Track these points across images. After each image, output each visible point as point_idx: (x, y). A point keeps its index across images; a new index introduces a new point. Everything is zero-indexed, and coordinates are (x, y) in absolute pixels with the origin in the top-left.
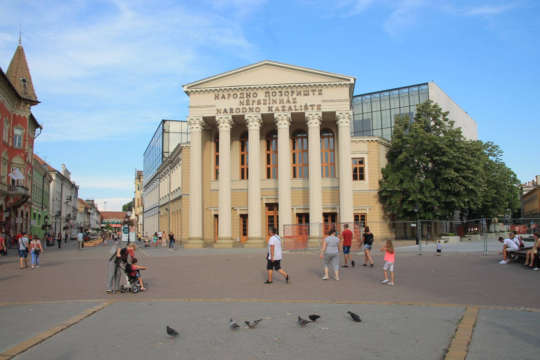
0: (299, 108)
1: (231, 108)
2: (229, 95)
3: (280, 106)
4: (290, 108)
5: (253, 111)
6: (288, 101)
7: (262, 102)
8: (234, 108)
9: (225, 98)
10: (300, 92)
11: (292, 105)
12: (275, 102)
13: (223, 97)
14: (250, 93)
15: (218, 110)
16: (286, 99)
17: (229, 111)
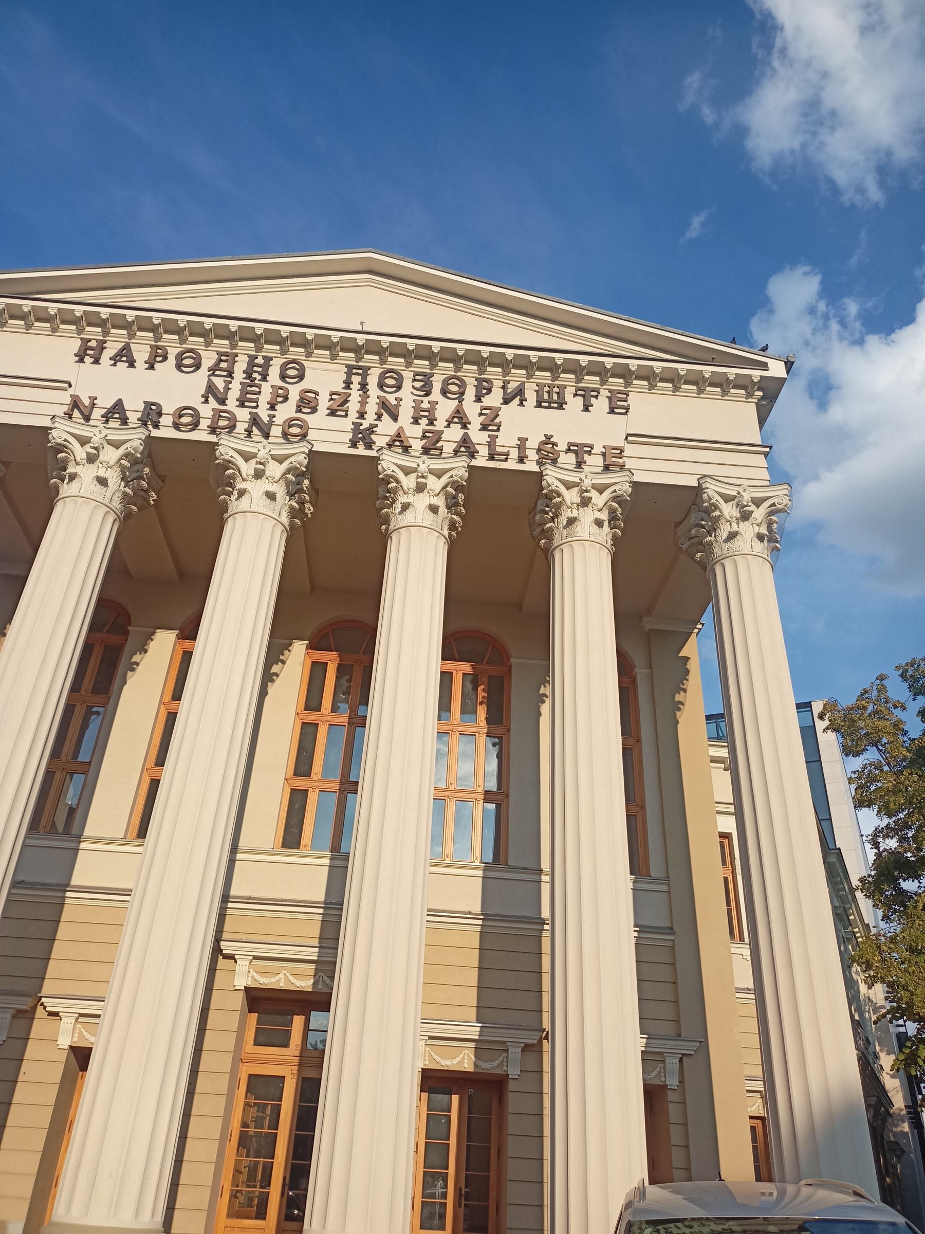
0: (514, 454)
1: (148, 404)
2: (157, 357)
3: (414, 433)
4: (466, 447)
5: (267, 436)
6: (459, 417)
7: (324, 403)
8: (169, 408)
9: (132, 364)
11: (479, 437)
12: (389, 410)
13: (125, 356)
14: (268, 360)
15: (76, 403)
16: (445, 408)
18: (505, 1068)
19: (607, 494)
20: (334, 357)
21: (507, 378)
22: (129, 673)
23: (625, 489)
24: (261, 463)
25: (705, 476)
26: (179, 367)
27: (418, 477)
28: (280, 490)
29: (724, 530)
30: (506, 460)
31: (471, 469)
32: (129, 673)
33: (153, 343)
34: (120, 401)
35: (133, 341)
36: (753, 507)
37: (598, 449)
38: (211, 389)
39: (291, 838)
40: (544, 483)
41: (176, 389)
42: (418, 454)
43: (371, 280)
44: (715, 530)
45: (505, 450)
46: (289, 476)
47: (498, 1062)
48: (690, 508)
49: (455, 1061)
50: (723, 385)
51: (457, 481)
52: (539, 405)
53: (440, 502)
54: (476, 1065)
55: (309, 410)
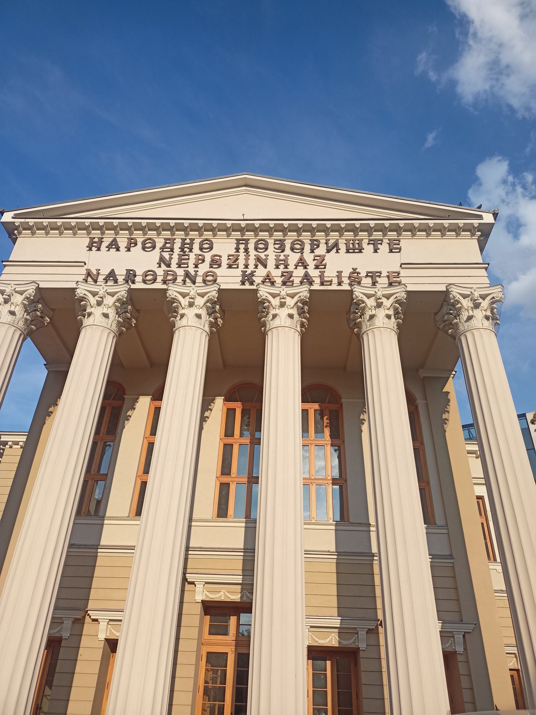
0: (335, 281)
1: (128, 271)
2: (131, 244)
3: (276, 274)
4: (307, 279)
7: (225, 262)
8: (140, 272)
9: (118, 249)
10: (336, 245)
11: (314, 273)
13: (114, 245)
14: (192, 240)
15: (89, 273)
16: (293, 258)
17: (121, 279)
18: (357, 644)
19: (392, 299)
20: (229, 235)
21: (328, 238)
22: (47, 417)
23: (403, 295)
24: (192, 298)
25: (450, 284)
26: (144, 248)
27: (281, 299)
28: (203, 312)
29: (465, 315)
30: (331, 284)
31: (311, 291)
32: (47, 417)
33: (129, 236)
34: (113, 270)
35: (104, 236)
36: (481, 300)
37: (384, 274)
38: (162, 259)
39: (222, 512)
40: (354, 296)
41: (143, 261)
42: (280, 286)
43: (247, 190)
44: (459, 315)
45: (330, 279)
46: (208, 304)
47: (352, 640)
48: (443, 304)
49: (327, 641)
50: (457, 230)
51: (303, 299)
52: (348, 252)
53: (294, 312)
54: (339, 643)
55: (217, 266)
